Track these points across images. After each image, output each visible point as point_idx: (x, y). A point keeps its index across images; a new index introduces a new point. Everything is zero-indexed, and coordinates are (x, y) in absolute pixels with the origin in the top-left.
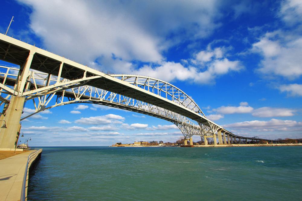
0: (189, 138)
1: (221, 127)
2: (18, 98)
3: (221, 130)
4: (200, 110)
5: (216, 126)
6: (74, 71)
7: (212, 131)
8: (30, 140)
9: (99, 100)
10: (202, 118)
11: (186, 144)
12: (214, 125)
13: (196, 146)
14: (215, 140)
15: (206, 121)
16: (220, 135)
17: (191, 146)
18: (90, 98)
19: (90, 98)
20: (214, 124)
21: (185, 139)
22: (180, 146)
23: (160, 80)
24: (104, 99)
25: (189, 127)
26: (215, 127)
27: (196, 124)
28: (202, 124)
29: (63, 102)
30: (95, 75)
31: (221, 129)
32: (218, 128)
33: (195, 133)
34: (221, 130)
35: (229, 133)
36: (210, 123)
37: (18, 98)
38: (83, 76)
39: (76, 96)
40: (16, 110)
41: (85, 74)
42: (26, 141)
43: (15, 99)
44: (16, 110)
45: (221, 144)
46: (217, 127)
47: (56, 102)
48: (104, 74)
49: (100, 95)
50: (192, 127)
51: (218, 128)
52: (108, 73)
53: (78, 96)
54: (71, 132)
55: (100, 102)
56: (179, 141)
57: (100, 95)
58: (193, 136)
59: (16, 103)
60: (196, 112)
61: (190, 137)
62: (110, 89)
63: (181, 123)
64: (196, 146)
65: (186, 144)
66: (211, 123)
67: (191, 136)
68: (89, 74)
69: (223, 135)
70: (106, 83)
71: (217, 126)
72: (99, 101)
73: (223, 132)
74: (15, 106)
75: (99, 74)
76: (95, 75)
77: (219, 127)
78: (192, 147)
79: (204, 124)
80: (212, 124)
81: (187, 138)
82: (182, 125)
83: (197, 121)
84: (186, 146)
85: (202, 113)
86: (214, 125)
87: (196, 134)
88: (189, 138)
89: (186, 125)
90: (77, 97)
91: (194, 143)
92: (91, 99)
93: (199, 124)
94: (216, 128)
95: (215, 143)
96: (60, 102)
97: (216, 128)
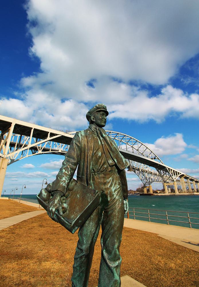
0: (149, 186)
1: (182, 174)
2: (4, 159)
3: (184, 176)
4: (156, 156)
5: (176, 172)
6: (40, 133)
7: (172, 178)
8: (17, 189)
9: (58, 151)
10: (159, 165)
11: (145, 192)
12: (174, 171)
13: (156, 194)
14: (166, 188)
15: (165, 167)
16: (183, 182)
17: (150, 195)
18: (50, 150)
19: (50, 150)
20: (174, 170)
21: (145, 186)
22: (139, 195)
23: (113, 132)
24: (62, 151)
25: (148, 174)
26: (176, 173)
27: (153, 170)
28: (161, 171)
29: (28, 155)
30: (57, 135)
31: (183, 175)
32: (179, 174)
33: (155, 180)
34: (184, 176)
35: (194, 180)
36: (169, 169)
37: (4, 159)
38: (47, 136)
39: (39, 148)
40: (3, 168)
41: (49, 134)
42: (12, 190)
43: (3, 160)
44: (3, 168)
45: (185, 192)
46: (178, 173)
47: (22, 155)
48: (64, 133)
49: (59, 146)
50: (152, 174)
51: (179, 174)
52: (66, 132)
53: (40, 149)
54: (30, 178)
55: (59, 153)
56: (139, 189)
57: (59, 146)
58: (153, 183)
59: (3, 163)
60: (152, 159)
61: (149, 185)
62: (68, 143)
63: (138, 170)
64: (156, 194)
65: (145, 192)
66: (170, 170)
67: (150, 183)
68: (52, 135)
69: (187, 181)
70: (65, 139)
71: (177, 173)
72: (58, 152)
73: (186, 178)
74: (3, 166)
75: (61, 134)
76: (57, 135)
77: (180, 174)
78: (152, 196)
79: (163, 171)
80: (171, 170)
81: (146, 186)
82: (140, 172)
83: (155, 167)
84: (146, 195)
85: (158, 159)
86: (174, 171)
87: (156, 181)
88: (149, 186)
89: (144, 172)
90: (39, 149)
91: (154, 192)
92: (51, 151)
93: (158, 170)
94: (177, 175)
95: (176, 192)
96: (26, 155)
97: (177, 175)
